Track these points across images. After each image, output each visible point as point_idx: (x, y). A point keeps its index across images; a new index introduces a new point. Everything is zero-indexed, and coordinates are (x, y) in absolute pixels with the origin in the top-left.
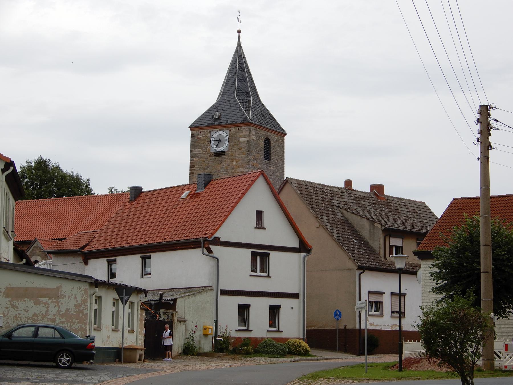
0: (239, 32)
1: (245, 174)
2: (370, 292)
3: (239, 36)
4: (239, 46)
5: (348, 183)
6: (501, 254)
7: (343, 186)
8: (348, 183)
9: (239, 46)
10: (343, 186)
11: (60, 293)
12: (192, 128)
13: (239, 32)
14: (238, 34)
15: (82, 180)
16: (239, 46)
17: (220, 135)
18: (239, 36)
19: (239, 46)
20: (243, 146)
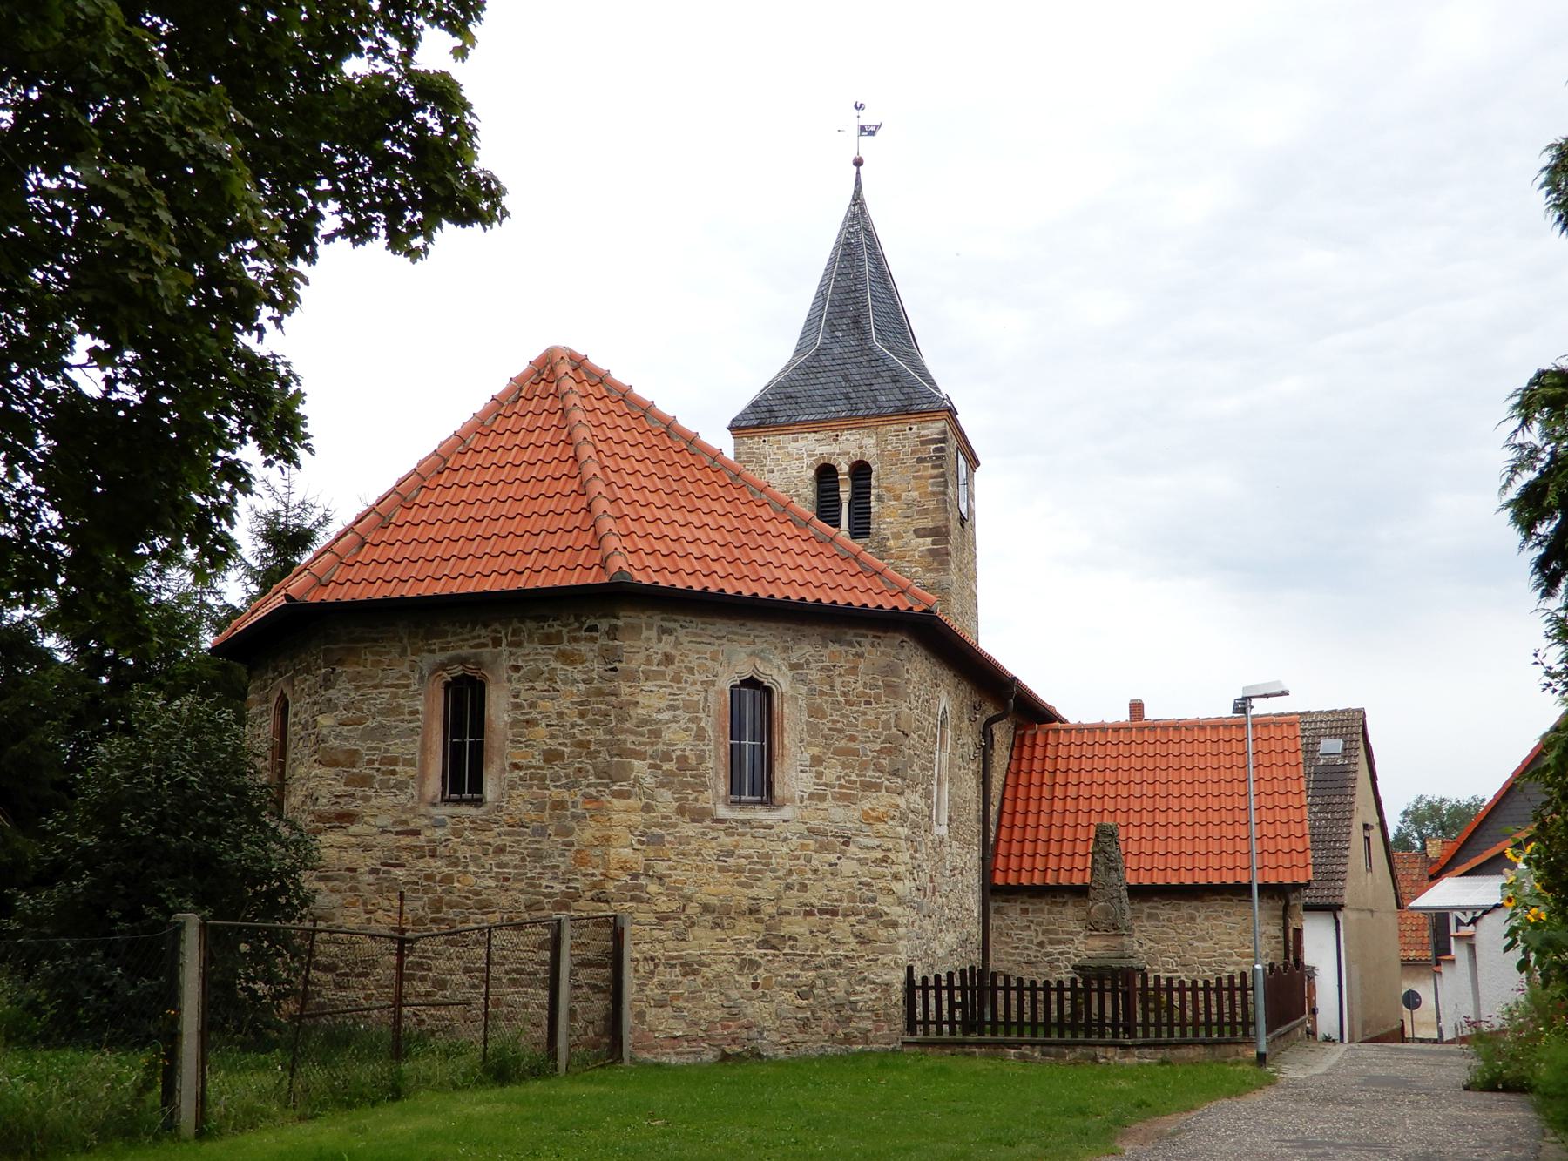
0: (858, 163)
1: (907, 1149)
2: (861, 471)
3: (858, 173)
4: (858, 216)
5: (1136, 708)
6: (436, 124)
7: (1123, 716)
8: (1136, 708)
9: (858, 216)
10: (1123, 716)
11: (633, 776)
12: (739, 428)
13: (858, 163)
14: (855, 168)
15: (303, 656)
16: (857, 199)
17: (93, 144)
18: (858, 173)
19: (857, 199)
20: (883, 582)
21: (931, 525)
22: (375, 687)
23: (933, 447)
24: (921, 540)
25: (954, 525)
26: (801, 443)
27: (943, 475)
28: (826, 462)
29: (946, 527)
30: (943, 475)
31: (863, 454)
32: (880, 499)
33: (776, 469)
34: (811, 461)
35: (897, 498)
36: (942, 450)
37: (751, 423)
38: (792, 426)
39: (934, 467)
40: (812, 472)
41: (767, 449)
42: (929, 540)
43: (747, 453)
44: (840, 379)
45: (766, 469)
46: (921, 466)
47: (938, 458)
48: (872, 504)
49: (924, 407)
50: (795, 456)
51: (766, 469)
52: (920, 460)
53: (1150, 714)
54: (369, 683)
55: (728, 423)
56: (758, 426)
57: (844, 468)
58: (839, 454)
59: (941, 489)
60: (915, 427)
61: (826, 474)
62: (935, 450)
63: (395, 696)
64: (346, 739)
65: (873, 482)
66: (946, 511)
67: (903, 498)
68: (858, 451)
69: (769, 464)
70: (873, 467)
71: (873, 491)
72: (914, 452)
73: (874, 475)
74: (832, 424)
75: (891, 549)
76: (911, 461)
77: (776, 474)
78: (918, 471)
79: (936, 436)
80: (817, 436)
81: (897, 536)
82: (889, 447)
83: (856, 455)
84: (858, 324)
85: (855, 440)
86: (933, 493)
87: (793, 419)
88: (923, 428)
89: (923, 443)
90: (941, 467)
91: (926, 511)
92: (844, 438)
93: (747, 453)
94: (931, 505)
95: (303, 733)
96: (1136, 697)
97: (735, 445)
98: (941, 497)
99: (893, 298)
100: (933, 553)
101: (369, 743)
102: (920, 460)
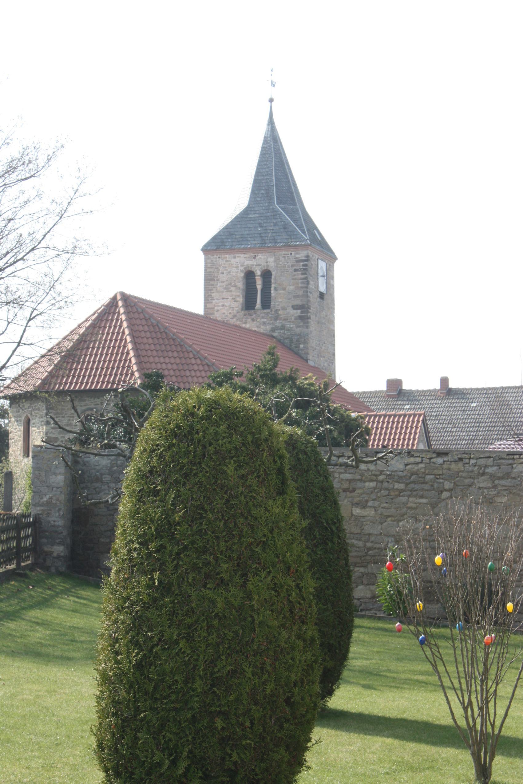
0: (271, 100)
2: (267, 275)
5: (444, 381)
8: (444, 381)
10: (438, 387)
13: (271, 100)
16: (271, 122)
19: (271, 122)
21: (300, 303)
22: (63, 417)
23: (302, 264)
24: (295, 311)
25: (314, 298)
26: (237, 260)
27: (306, 278)
28: (250, 269)
29: (308, 305)
30: (306, 278)
31: (268, 266)
32: (276, 289)
33: (225, 272)
34: (242, 268)
35: (284, 289)
36: (306, 265)
37: (213, 248)
38: (232, 250)
39: (302, 274)
40: (242, 275)
41: (220, 261)
42: (299, 311)
43: (210, 263)
44: (257, 225)
45: (220, 272)
46: (296, 273)
47: (304, 269)
48: (272, 292)
49: (298, 243)
50: (235, 266)
51: (220, 272)
52: (295, 270)
53: (452, 385)
54: (61, 416)
55: (201, 248)
56: (216, 250)
57: (258, 273)
58: (256, 265)
59: (305, 285)
60: (293, 253)
61: (249, 275)
62: (303, 265)
63: (69, 420)
64: (54, 434)
65: (273, 281)
66: (307, 296)
67: (287, 289)
68: (265, 264)
69: (221, 269)
70: (273, 273)
71: (273, 286)
72: (292, 266)
73: (273, 277)
74: (255, 250)
75: (280, 315)
76: (291, 270)
77: (225, 274)
78: (295, 275)
79: (304, 258)
80: (245, 256)
81: (284, 309)
82: (281, 263)
83: (264, 266)
84: (269, 197)
85: (265, 258)
86: (302, 287)
87: (233, 247)
88: (298, 254)
89: (297, 261)
90: (306, 274)
91: (298, 296)
92: (259, 257)
93: (210, 263)
94: (300, 293)
95: (37, 431)
96: (444, 375)
97: (205, 259)
98: (305, 289)
99: (287, 177)
100: (301, 318)
101: (61, 435)
102: (295, 270)
